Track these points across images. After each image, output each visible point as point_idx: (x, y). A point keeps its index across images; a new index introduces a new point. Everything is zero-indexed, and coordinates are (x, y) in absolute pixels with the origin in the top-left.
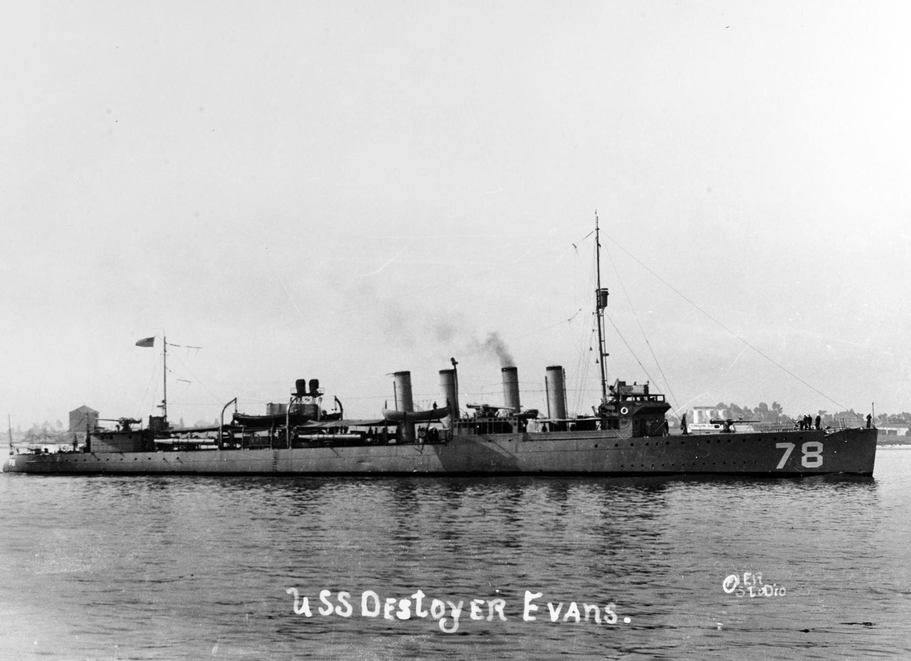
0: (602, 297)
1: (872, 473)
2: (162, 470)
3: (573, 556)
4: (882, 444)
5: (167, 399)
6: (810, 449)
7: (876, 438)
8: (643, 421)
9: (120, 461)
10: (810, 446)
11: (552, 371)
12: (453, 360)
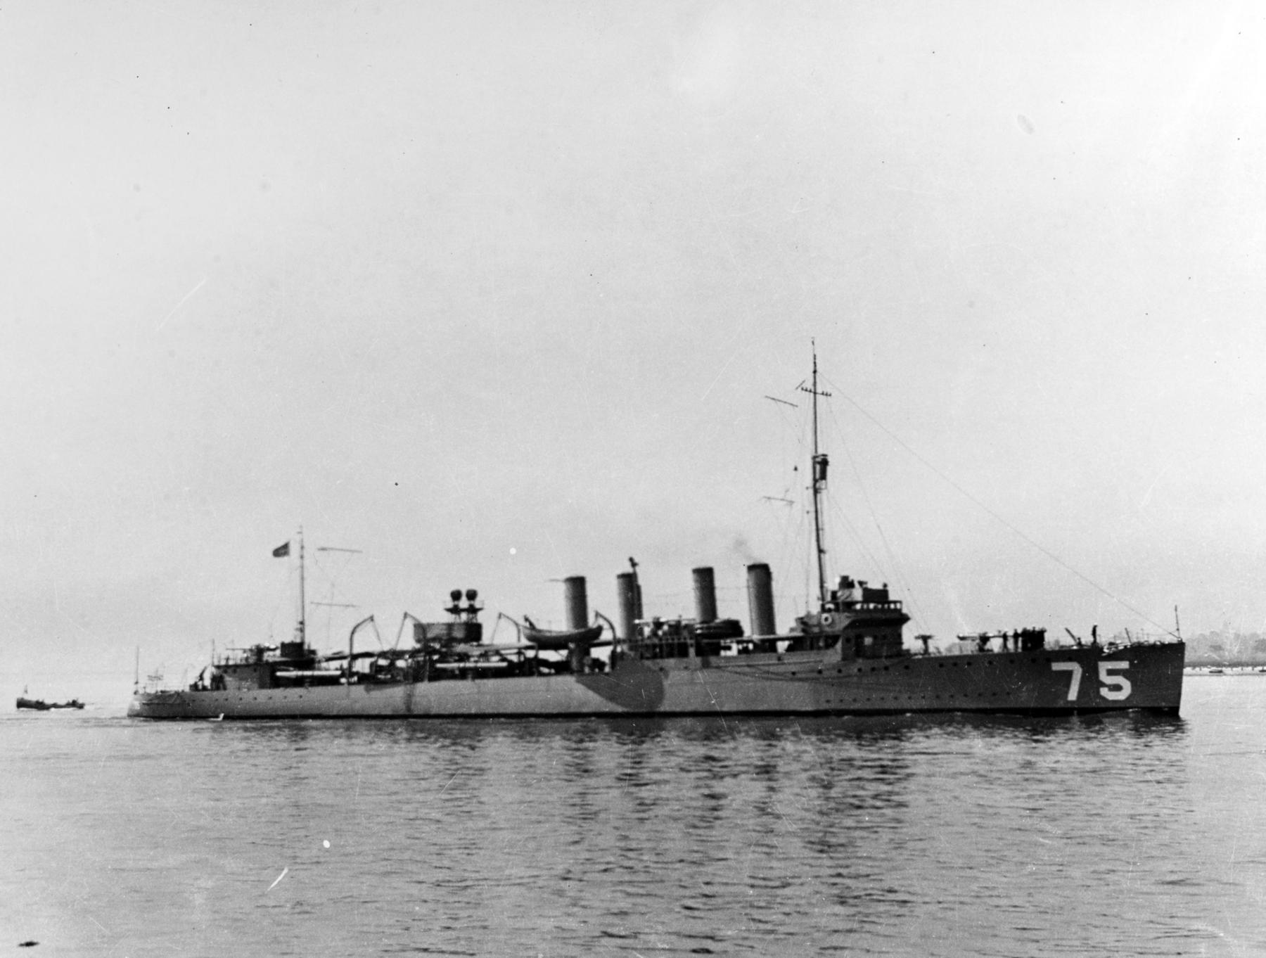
0: (821, 465)
1: (1177, 709)
5: (306, 617)
7: (1182, 657)
8: (860, 638)
9: (299, 699)
10: (1110, 667)
11: (758, 570)
12: (631, 560)
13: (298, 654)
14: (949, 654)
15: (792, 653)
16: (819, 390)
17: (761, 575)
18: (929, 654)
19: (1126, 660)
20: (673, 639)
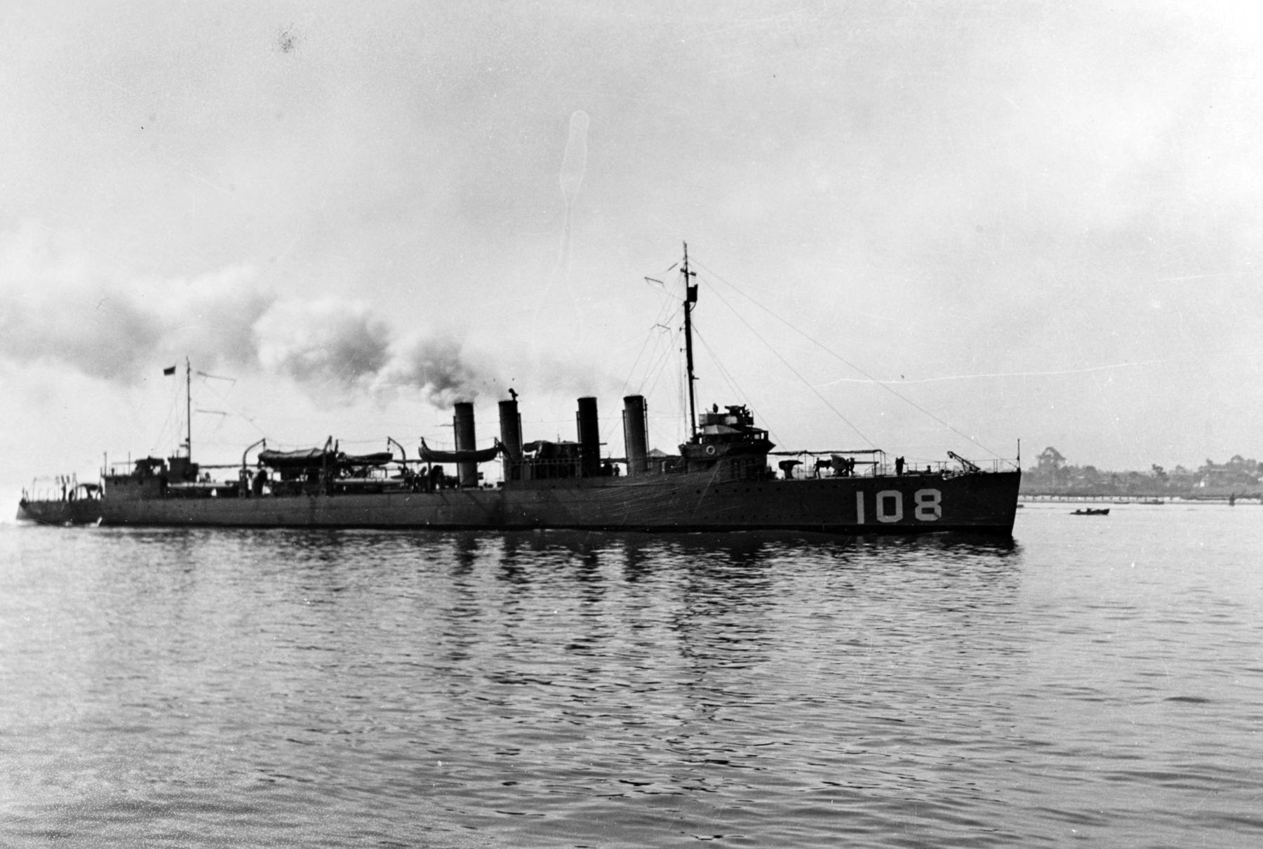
2: (205, 520)
3: (430, 681)
4: (1025, 494)
6: (925, 498)
13: (184, 468)
14: (209, 530)
15: (711, 469)
16: (689, 271)
17: (635, 408)
18: (792, 478)
19: (856, 493)
20: (561, 461)
